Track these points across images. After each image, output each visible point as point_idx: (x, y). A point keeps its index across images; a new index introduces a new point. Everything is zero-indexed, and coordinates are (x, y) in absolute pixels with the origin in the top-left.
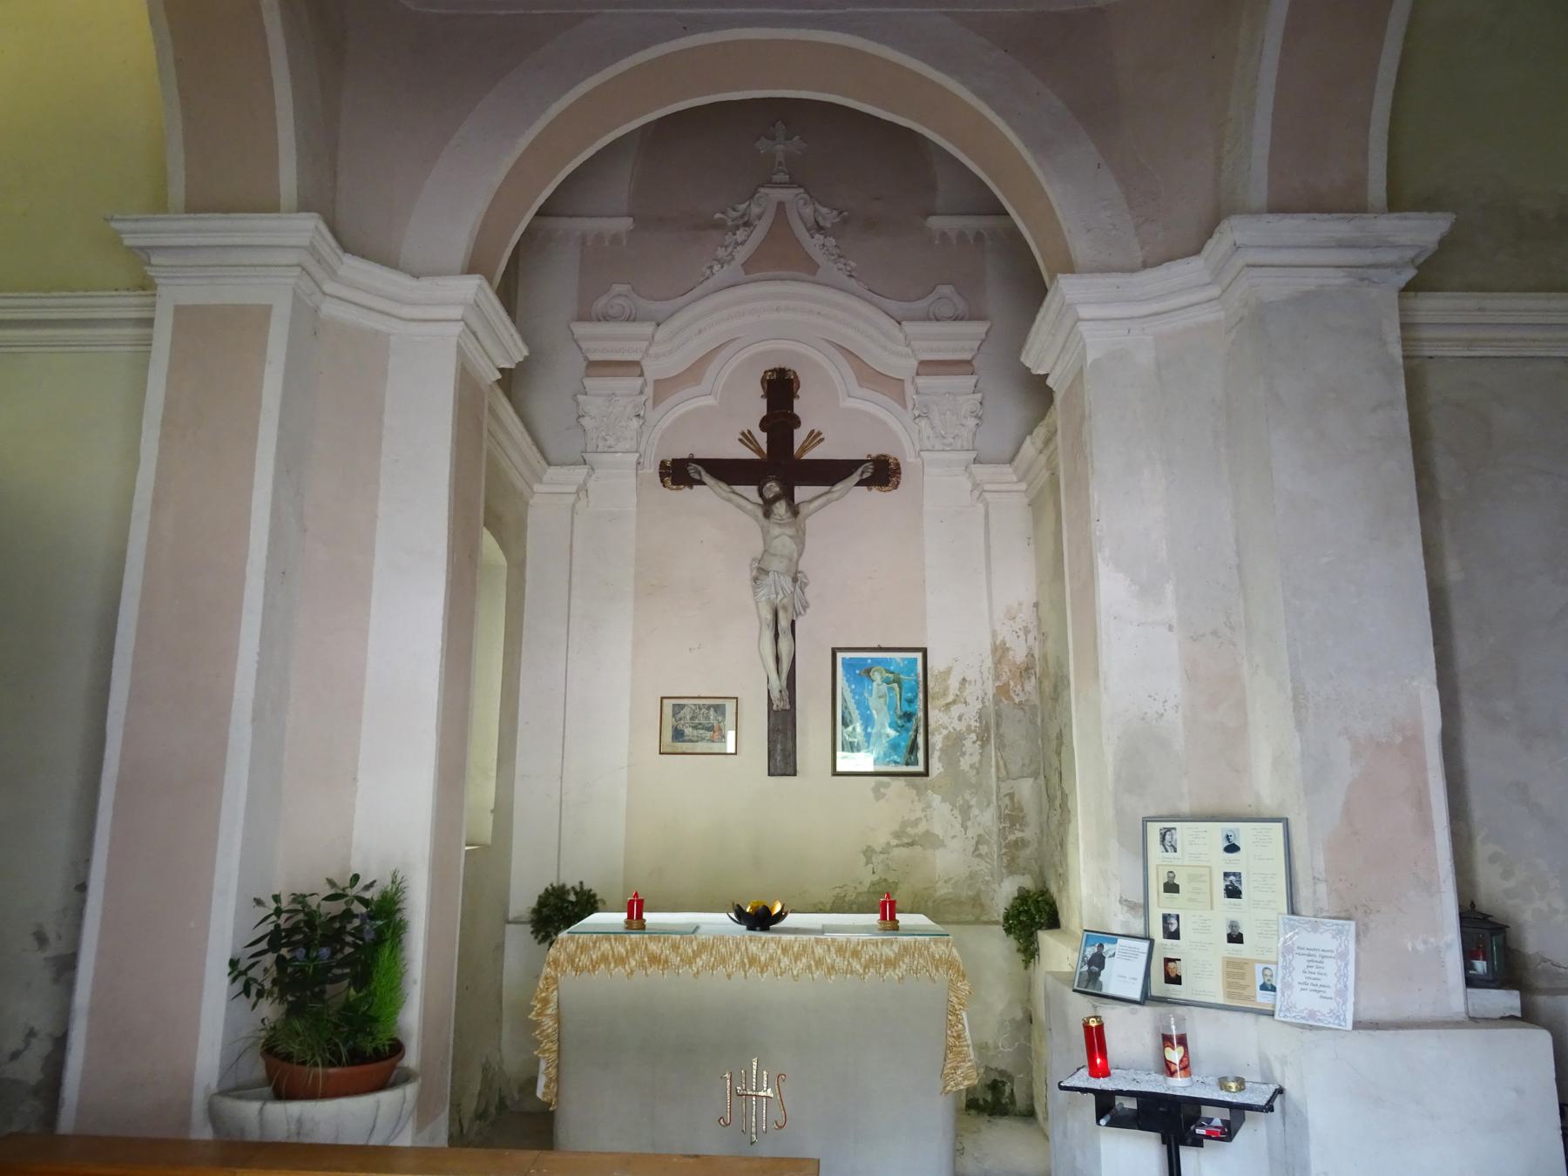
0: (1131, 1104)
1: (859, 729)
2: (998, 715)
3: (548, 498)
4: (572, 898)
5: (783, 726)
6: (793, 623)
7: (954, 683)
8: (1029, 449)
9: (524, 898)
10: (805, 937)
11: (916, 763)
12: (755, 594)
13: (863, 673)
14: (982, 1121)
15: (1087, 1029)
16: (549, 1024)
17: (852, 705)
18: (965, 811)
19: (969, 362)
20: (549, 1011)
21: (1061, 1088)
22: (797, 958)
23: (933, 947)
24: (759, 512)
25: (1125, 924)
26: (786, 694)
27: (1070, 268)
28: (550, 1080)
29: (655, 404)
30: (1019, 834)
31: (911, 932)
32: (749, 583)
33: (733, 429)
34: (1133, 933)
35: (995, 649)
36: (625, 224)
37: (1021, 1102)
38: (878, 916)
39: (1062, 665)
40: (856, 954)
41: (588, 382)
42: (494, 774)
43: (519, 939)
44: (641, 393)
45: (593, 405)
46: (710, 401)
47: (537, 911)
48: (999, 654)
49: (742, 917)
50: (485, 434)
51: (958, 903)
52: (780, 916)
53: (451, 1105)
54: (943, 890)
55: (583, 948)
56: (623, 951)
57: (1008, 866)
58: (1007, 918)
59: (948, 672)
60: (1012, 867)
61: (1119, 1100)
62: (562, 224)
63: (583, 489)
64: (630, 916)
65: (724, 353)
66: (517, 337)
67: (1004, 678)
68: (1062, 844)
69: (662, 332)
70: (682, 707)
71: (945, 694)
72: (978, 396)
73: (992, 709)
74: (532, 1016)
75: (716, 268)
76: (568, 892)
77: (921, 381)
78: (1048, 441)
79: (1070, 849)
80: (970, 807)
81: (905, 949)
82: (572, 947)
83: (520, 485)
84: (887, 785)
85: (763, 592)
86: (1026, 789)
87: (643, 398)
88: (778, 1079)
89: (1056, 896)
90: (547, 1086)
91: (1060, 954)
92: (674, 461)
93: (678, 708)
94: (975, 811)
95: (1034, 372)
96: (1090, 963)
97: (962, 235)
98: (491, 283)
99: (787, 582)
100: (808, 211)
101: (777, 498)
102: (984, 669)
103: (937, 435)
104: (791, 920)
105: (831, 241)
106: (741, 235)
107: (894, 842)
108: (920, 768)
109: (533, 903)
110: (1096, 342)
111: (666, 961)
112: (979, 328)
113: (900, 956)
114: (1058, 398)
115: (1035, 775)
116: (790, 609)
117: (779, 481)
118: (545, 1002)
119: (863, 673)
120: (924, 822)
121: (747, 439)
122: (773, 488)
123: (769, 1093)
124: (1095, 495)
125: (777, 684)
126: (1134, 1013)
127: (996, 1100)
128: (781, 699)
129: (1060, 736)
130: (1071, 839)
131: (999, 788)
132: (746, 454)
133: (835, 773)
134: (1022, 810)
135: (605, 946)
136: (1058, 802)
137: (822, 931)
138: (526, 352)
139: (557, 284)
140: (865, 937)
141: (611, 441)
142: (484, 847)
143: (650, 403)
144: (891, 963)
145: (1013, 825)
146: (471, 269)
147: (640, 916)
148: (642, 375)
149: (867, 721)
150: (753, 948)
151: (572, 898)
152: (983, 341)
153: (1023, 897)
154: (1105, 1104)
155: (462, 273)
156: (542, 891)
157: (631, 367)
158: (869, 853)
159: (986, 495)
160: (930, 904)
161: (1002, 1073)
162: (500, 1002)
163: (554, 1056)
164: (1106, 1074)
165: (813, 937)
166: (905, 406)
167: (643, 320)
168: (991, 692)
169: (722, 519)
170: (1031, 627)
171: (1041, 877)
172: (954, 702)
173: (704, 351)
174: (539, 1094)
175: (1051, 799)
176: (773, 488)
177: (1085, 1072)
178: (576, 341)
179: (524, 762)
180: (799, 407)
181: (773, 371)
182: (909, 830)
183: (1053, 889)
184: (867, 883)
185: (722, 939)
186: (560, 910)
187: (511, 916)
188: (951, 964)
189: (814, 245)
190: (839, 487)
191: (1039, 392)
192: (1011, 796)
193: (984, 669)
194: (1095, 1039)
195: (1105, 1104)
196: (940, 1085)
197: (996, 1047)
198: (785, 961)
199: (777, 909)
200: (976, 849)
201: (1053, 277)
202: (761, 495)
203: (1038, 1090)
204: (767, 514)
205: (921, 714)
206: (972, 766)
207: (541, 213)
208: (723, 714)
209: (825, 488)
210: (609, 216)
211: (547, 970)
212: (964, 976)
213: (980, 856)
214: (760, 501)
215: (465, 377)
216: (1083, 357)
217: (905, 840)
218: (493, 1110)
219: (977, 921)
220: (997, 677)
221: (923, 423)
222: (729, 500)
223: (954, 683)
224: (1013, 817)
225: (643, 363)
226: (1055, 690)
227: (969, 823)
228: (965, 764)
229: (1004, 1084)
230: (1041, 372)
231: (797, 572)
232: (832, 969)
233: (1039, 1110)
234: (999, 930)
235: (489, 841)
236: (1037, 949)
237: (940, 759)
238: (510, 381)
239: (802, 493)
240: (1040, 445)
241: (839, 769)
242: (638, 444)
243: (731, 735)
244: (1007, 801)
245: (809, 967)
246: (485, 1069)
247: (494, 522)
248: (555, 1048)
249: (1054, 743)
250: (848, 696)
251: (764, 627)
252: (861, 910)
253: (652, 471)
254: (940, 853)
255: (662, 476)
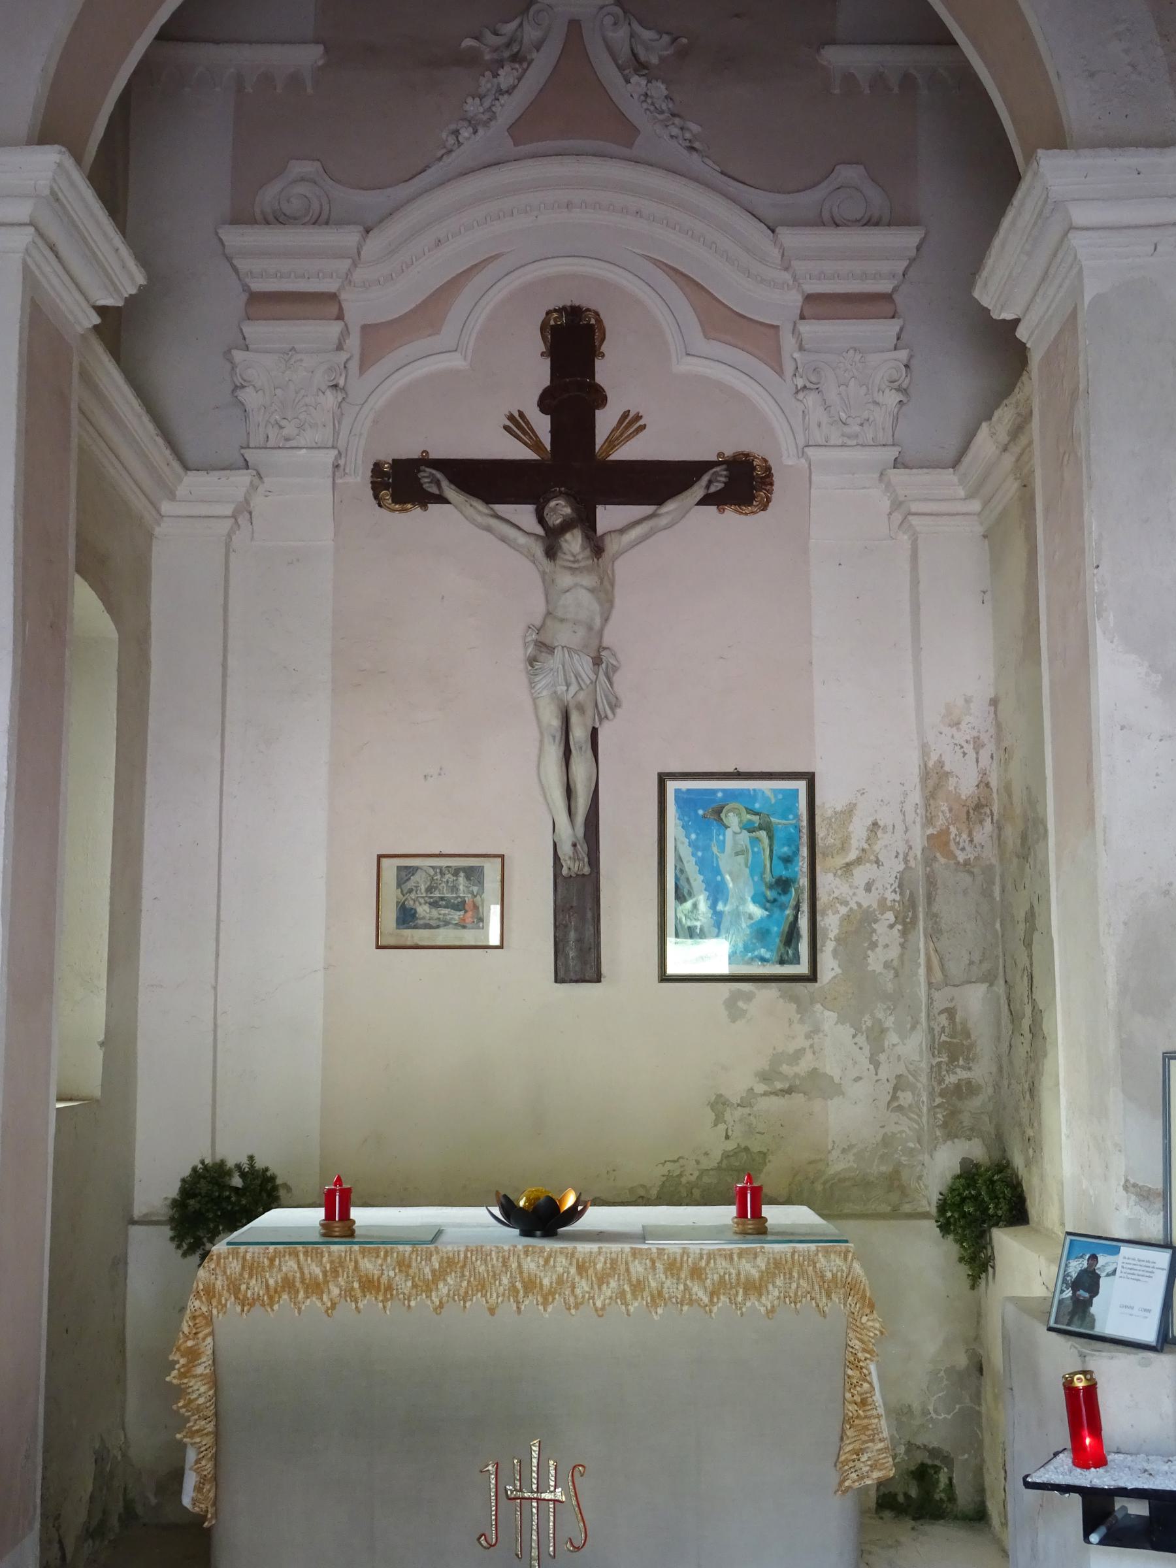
0: (1139, 1509)
1: (703, 906)
2: (931, 880)
3: (187, 524)
4: (237, 1181)
5: (578, 903)
6: (594, 733)
7: (858, 830)
8: (986, 443)
9: (157, 1181)
10: (615, 1247)
11: (796, 960)
12: (532, 684)
13: (708, 814)
14: (903, 1530)
15: (1071, 1392)
16: (200, 1391)
17: (691, 867)
18: (876, 1037)
19: (887, 297)
20: (199, 1370)
21: (1028, 1485)
22: (602, 1280)
23: (822, 1261)
24: (538, 550)
25: (1132, 1222)
26: (583, 849)
27: (1058, 140)
28: (203, 1480)
29: (363, 367)
30: (963, 1074)
31: (788, 1236)
32: (521, 665)
33: (490, 406)
34: (1145, 1236)
35: (925, 775)
36: (309, 56)
37: (964, 1497)
38: (732, 1210)
39: (1034, 801)
40: (697, 1273)
41: (249, 329)
42: (103, 983)
43: (150, 1251)
44: (340, 348)
45: (259, 367)
46: (457, 362)
47: (179, 1205)
48: (931, 783)
49: (511, 1213)
50: (75, 414)
51: (865, 1184)
52: (574, 1214)
53: (44, 1516)
54: (839, 1165)
55: (253, 1269)
56: (317, 1271)
57: (945, 1125)
58: (942, 1208)
59: (850, 811)
60: (951, 1128)
61: (1119, 1503)
62: (202, 55)
63: (244, 510)
64: (329, 1216)
65: (480, 280)
66: (124, 251)
67: (940, 822)
68: (1033, 1090)
69: (375, 244)
70: (412, 870)
71: (844, 848)
72: (903, 355)
73: (920, 872)
74: (172, 1378)
75: (465, 133)
76: (229, 1173)
77: (805, 328)
78: (1018, 430)
79: (1046, 1096)
80: (883, 1031)
81: (777, 1265)
82: (235, 1266)
83: (139, 503)
84: (749, 997)
85: (542, 682)
86: (975, 1001)
87: (344, 356)
88: (573, 1473)
89: (1022, 1171)
90: (198, 1489)
91: (1027, 1267)
92: (396, 463)
93: (405, 874)
94: (892, 1038)
95: (995, 315)
96: (1076, 1285)
97: (878, 80)
98: (79, 160)
99: (584, 665)
100: (619, 35)
101: (566, 526)
102: (909, 808)
103: (834, 418)
104: (595, 1218)
105: (659, 89)
106: (506, 77)
107: (760, 1088)
108: (803, 968)
109: (173, 1191)
110: (1100, 266)
111: (389, 1288)
112: (908, 239)
113: (768, 1276)
114: (1035, 359)
115: (989, 978)
116: (590, 711)
117: (573, 497)
118: (193, 1355)
119: (708, 814)
120: (809, 1056)
121: (517, 425)
122: (560, 509)
123: (559, 1494)
124: (1093, 525)
125: (568, 833)
126: (1147, 1364)
127: (925, 1494)
128: (576, 857)
129: (1031, 916)
130: (1046, 1082)
131: (930, 1001)
132: (516, 451)
133: (664, 978)
134: (968, 1036)
135: (290, 1265)
136: (1026, 1023)
137: (643, 1237)
138: (141, 280)
139: (195, 163)
140: (710, 1245)
141: (290, 429)
142: (90, 1101)
143: (354, 366)
144: (754, 1287)
145: (953, 1059)
146: (43, 136)
147: (345, 1215)
148: (340, 317)
149: (717, 892)
150: (531, 1265)
151: (237, 1181)
152: (912, 261)
153: (969, 1174)
154: (1098, 1511)
155: (29, 142)
156: (187, 1172)
157: (323, 304)
158: (719, 1105)
159: (914, 520)
160: (819, 1187)
161: (934, 1452)
162: (123, 1352)
163: (208, 1441)
164: (1100, 1461)
165: (627, 1247)
166: (780, 372)
167: (342, 223)
168: (918, 843)
169: (477, 556)
170: (985, 738)
171: (999, 1141)
172: (859, 861)
173: (450, 270)
174: (186, 1501)
175: (1015, 1017)
176: (560, 509)
177: (1066, 1459)
178: (229, 259)
179: (152, 965)
180: (604, 373)
181: (561, 310)
182: (785, 1068)
183: (1018, 1161)
184: (717, 1155)
185: (480, 1252)
186: (217, 1202)
187: (138, 1211)
188: (851, 1287)
189: (629, 94)
190: (671, 506)
191: (1002, 351)
192: (950, 1012)
193: (909, 808)
194: (1083, 1407)
195: (1098, 1511)
196: (834, 1478)
197: (925, 1412)
198: (583, 1286)
199: (570, 1200)
200: (894, 1097)
201: (1030, 156)
202: (541, 520)
203: (992, 1478)
204: (551, 552)
205: (804, 881)
206: (887, 965)
207: (163, 36)
208: (481, 883)
209: (648, 509)
210: (283, 43)
211: (195, 1304)
212: (872, 1306)
213: (900, 1108)
214: (540, 531)
215: (39, 322)
216: (1077, 290)
217: (779, 1085)
218: (114, 1521)
219: (895, 1214)
220: (929, 821)
221: (811, 399)
222: (488, 529)
223: (858, 830)
224: (953, 1046)
225: (343, 296)
226: (1025, 843)
227: (882, 1057)
228: (875, 961)
229: (937, 1469)
230: (1008, 316)
231: (601, 648)
232: (658, 1297)
233: (993, 1508)
234: (930, 1227)
235: (97, 1093)
236: (991, 1258)
237: (835, 953)
238: (117, 327)
239: (608, 516)
240: (1003, 437)
241: (671, 970)
242: (336, 433)
243: (495, 911)
244: (943, 1020)
245: (622, 1294)
246: (100, 1458)
247: (94, 565)
248: (210, 1427)
249: (1021, 927)
250: (686, 852)
251: (547, 739)
252: (707, 1199)
253: (359, 479)
254: (834, 1104)
255: (376, 488)
